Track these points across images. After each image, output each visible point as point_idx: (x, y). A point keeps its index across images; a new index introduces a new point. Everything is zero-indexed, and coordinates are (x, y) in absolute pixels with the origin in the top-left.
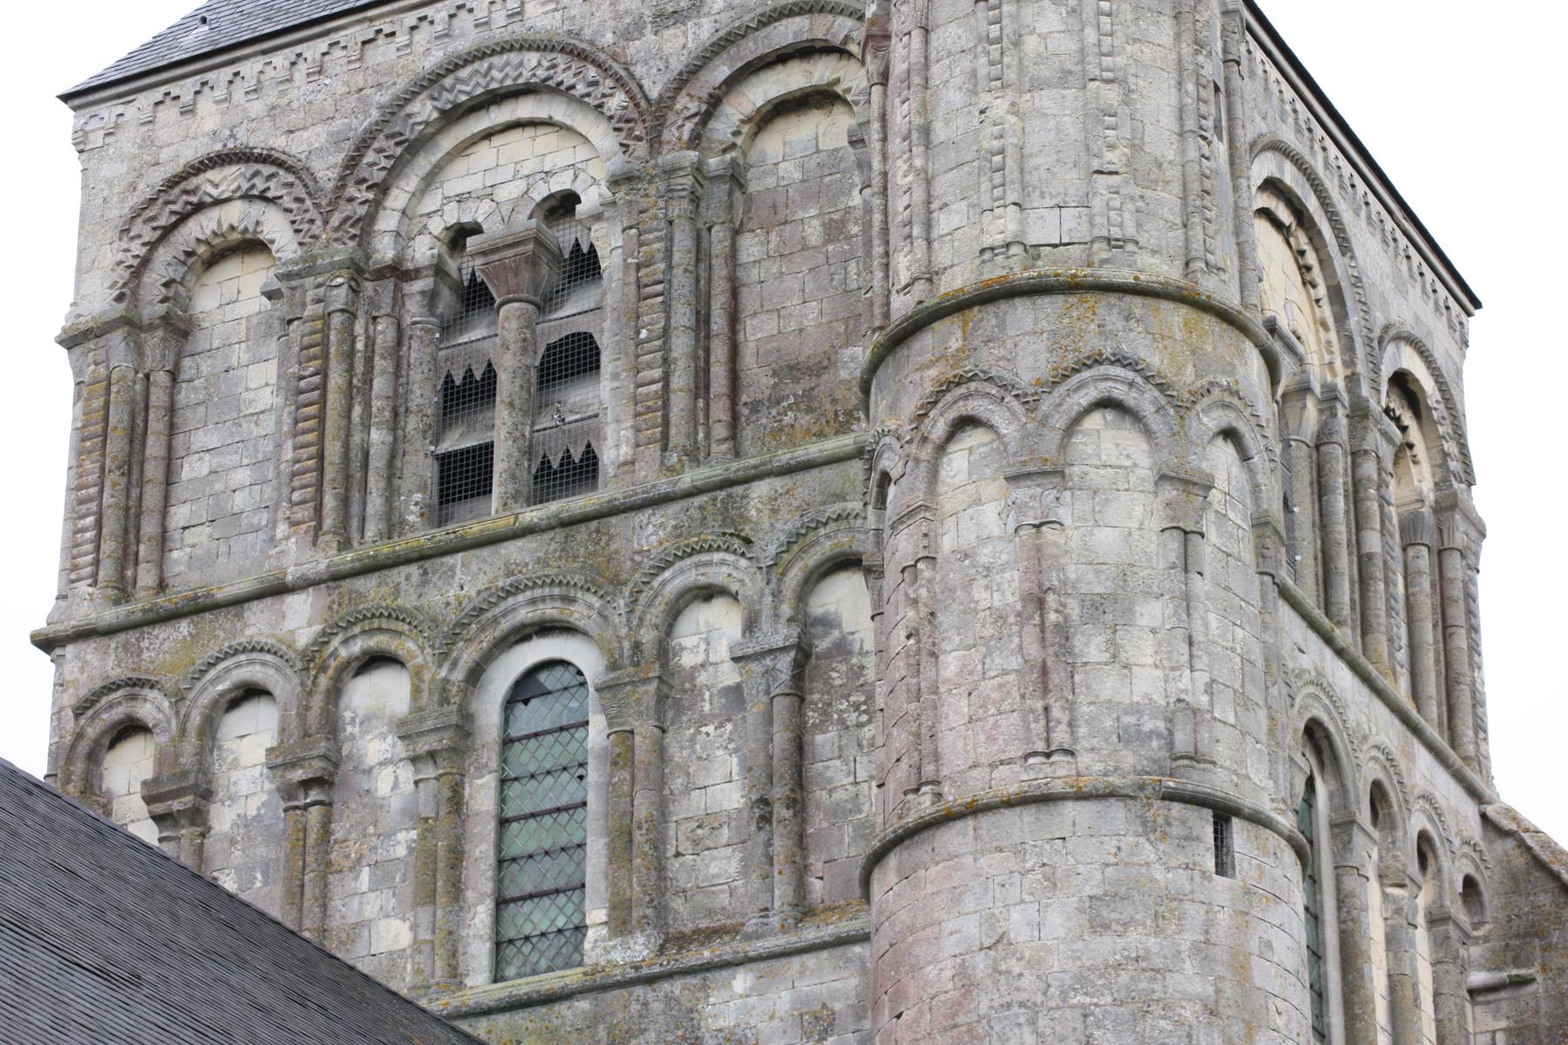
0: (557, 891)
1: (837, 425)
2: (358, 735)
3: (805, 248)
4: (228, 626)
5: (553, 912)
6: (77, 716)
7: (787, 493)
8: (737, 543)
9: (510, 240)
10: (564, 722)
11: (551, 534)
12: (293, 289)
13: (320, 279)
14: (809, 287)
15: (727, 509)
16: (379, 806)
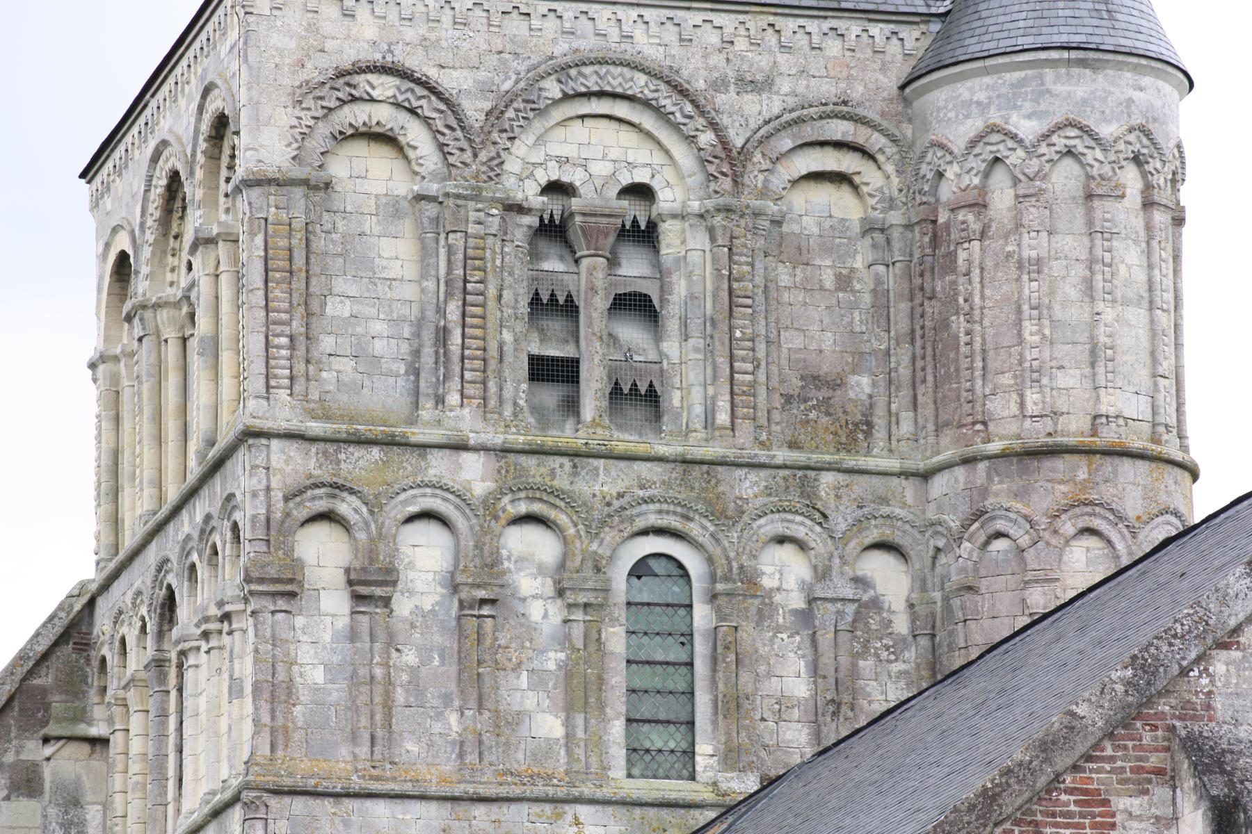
0: (668, 722)
1: (848, 431)
2: (513, 569)
3: (822, 288)
4: (414, 462)
5: (666, 737)
6: (287, 499)
7: (847, 486)
8: (817, 515)
9: (607, 211)
10: (670, 601)
11: (673, 465)
12: (458, 206)
13: (480, 206)
14: (826, 320)
15: (803, 485)
16: (531, 629)
